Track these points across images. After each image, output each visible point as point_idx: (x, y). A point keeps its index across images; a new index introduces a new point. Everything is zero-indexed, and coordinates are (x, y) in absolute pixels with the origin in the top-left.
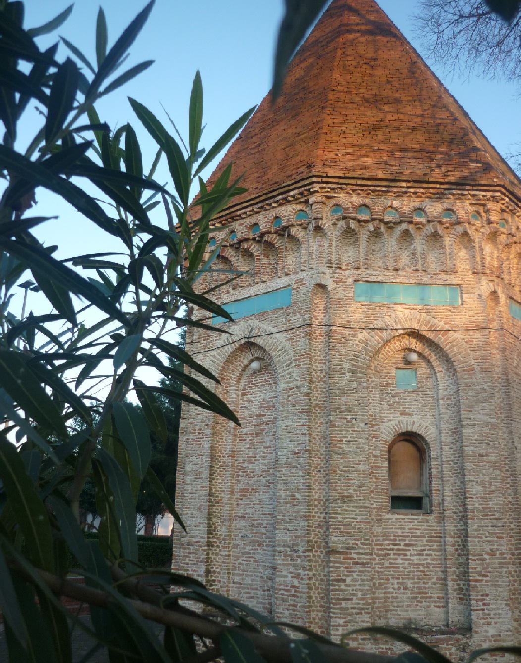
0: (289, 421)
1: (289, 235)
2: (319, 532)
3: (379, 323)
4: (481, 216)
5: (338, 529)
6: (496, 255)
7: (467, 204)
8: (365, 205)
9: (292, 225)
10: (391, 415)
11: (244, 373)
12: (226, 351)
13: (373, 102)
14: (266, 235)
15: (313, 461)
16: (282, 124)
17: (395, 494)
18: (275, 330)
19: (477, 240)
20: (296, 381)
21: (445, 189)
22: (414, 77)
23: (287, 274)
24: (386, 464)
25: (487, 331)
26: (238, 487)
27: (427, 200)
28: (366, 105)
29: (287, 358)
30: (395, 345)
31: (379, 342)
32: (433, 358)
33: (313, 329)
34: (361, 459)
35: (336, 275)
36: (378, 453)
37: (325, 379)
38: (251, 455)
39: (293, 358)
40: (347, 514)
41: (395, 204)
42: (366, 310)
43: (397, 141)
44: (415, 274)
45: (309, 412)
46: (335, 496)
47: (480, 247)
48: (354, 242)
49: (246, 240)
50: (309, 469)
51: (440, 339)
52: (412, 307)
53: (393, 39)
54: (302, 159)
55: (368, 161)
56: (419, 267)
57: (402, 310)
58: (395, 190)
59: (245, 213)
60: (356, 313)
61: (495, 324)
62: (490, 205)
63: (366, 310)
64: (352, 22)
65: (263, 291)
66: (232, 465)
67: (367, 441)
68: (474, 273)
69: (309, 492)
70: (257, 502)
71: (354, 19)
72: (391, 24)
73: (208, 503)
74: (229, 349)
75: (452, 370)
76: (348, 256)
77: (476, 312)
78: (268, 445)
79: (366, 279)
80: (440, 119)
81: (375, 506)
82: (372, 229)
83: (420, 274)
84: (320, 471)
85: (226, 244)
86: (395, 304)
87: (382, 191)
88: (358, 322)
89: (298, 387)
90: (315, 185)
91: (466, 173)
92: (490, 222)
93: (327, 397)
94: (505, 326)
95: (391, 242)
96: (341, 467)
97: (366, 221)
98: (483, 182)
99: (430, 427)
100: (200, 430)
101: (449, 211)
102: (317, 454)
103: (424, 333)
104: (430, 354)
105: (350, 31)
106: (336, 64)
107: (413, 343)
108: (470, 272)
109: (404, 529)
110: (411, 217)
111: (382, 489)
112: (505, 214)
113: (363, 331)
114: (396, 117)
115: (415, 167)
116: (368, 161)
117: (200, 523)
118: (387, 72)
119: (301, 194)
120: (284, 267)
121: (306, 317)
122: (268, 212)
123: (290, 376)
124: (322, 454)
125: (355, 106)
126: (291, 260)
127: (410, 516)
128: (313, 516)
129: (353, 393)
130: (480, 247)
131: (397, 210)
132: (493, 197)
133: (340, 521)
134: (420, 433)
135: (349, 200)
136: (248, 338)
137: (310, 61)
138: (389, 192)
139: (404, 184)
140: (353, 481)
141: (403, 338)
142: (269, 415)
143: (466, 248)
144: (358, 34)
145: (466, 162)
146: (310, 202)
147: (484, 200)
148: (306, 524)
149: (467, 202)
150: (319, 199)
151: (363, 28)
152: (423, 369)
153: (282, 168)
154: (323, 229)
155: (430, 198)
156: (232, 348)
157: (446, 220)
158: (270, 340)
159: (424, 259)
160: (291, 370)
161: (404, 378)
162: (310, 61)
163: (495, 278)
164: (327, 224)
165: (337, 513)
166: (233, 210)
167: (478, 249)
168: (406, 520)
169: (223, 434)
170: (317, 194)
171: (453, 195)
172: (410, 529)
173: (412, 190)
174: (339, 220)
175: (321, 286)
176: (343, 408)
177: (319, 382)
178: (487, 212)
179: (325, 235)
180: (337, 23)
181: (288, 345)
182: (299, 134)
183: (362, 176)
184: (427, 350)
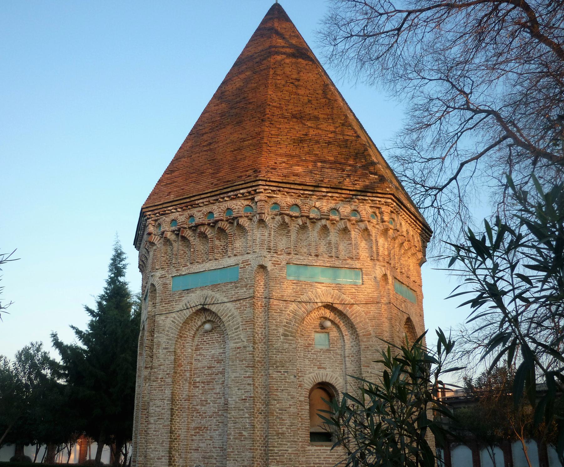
0: (236, 373)
1: (238, 224)
2: (260, 462)
3: (304, 298)
4: (376, 216)
5: (275, 459)
6: (386, 246)
7: (367, 207)
8: (296, 205)
9: (241, 217)
10: (311, 369)
11: (197, 332)
12: (184, 314)
13: (299, 117)
14: (220, 222)
15: (256, 405)
16: (229, 127)
17: (313, 430)
18: (225, 300)
19: (374, 234)
20: (243, 341)
21: (353, 195)
22: (326, 98)
23: (235, 255)
24: (308, 407)
25: (380, 305)
26: (193, 425)
27: (340, 202)
28: (294, 120)
29: (235, 323)
30: (315, 315)
31: (304, 313)
32: (342, 325)
33: (256, 301)
34: (291, 403)
35: (274, 259)
36: (302, 399)
37: (264, 341)
38: (203, 399)
39: (241, 323)
40: (282, 447)
41: (318, 204)
42: (295, 287)
43: (318, 153)
44: (330, 260)
45: (253, 367)
46: (273, 433)
47: (376, 240)
48: (287, 233)
49: (203, 224)
50: (253, 412)
51: (348, 311)
52: (327, 285)
53: (311, 63)
54: (250, 163)
55: (299, 169)
56: (333, 254)
57: (320, 287)
58: (318, 194)
59: (203, 203)
60: (288, 290)
61: (385, 299)
62: (384, 208)
63: (295, 287)
64: (278, 45)
65: (215, 267)
66: (188, 408)
67: (295, 389)
68: (371, 259)
69: (253, 430)
70: (209, 438)
71: (280, 42)
72: (308, 49)
73: (169, 440)
74: (188, 313)
75: (355, 334)
76: (282, 243)
77: (372, 290)
78: (218, 392)
79: (295, 263)
80: (347, 135)
81: (300, 440)
82: (301, 223)
83: (333, 259)
84: (261, 413)
85: (186, 226)
86: (316, 283)
87: (309, 194)
88: (290, 296)
89: (245, 347)
90: (261, 187)
91: (367, 183)
92: (383, 221)
93: (266, 355)
94: (392, 301)
95: (314, 233)
96: (277, 410)
97: (296, 217)
98: (379, 191)
99: (339, 378)
100: (162, 378)
101: (355, 211)
102: (259, 400)
103: (336, 306)
104: (339, 322)
105: (278, 53)
106: (270, 82)
107: (328, 313)
108: (369, 259)
109: (320, 458)
110: (329, 216)
111: (305, 427)
112: (393, 214)
113: (293, 303)
114: (316, 131)
115: (332, 175)
116: (299, 169)
117: (162, 456)
118: (308, 92)
119: (249, 192)
120: (233, 249)
121: (251, 291)
122: (221, 204)
123: (237, 338)
124: (262, 400)
125: (286, 120)
126: (239, 244)
127: (324, 448)
128: (257, 449)
129: (286, 352)
130: (376, 240)
131: (318, 209)
132: (386, 202)
133: (276, 453)
134: (331, 383)
135: (285, 200)
136: (203, 305)
137: (248, 73)
138: (313, 195)
139: (324, 190)
140: (286, 421)
141: (320, 309)
142: (219, 367)
143: (366, 240)
144: (284, 56)
145: (367, 174)
146: (256, 199)
147: (379, 204)
148: (251, 455)
149: (368, 205)
150: (263, 198)
151: (288, 50)
152: (334, 333)
153: (233, 169)
154: (265, 221)
155: (342, 201)
156: (190, 312)
157: (353, 218)
158: (221, 307)
159: (337, 248)
160: (238, 333)
161: (319, 339)
162: (248, 73)
163: (386, 264)
164: (267, 218)
165: (274, 447)
166: (193, 199)
167: (374, 241)
168: (322, 451)
169: (181, 382)
170: (261, 194)
171: (358, 199)
172: (325, 458)
173: (330, 194)
174: (276, 215)
175: (263, 267)
176: (278, 364)
177: (260, 343)
178: (381, 213)
179: (266, 226)
180: (267, 45)
181: (236, 313)
182: (244, 140)
183: (296, 182)
184: (337, 318)
